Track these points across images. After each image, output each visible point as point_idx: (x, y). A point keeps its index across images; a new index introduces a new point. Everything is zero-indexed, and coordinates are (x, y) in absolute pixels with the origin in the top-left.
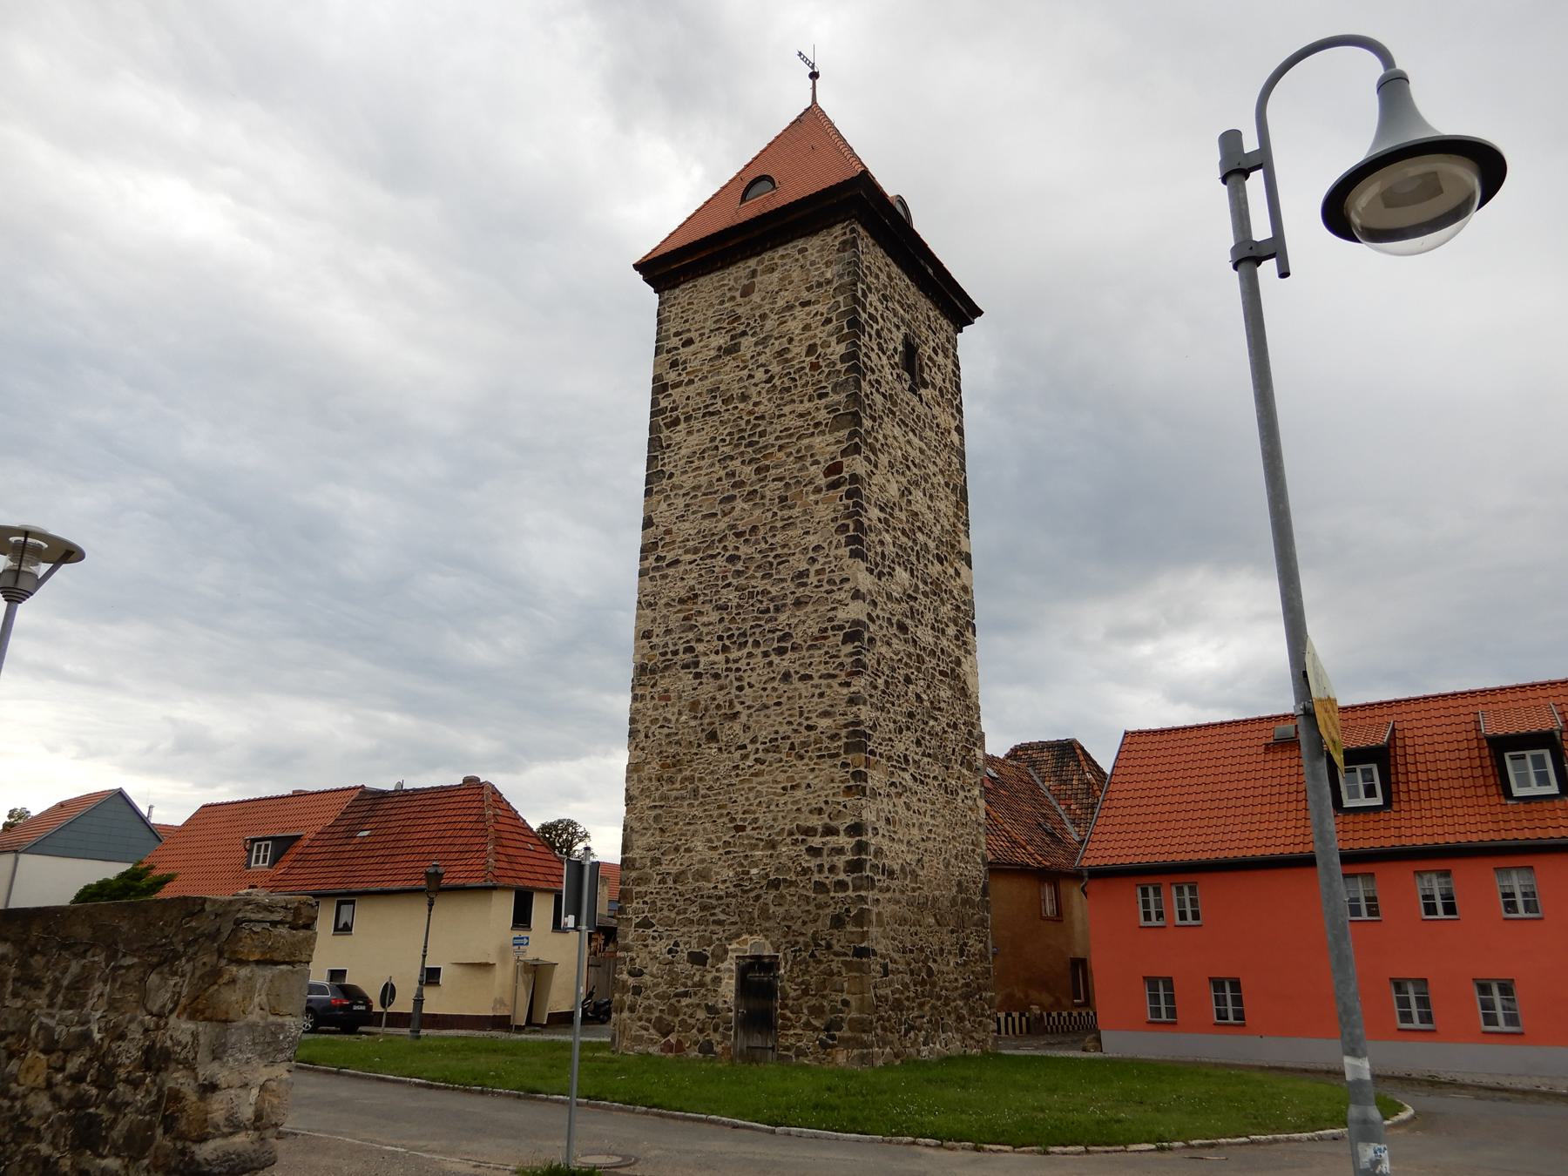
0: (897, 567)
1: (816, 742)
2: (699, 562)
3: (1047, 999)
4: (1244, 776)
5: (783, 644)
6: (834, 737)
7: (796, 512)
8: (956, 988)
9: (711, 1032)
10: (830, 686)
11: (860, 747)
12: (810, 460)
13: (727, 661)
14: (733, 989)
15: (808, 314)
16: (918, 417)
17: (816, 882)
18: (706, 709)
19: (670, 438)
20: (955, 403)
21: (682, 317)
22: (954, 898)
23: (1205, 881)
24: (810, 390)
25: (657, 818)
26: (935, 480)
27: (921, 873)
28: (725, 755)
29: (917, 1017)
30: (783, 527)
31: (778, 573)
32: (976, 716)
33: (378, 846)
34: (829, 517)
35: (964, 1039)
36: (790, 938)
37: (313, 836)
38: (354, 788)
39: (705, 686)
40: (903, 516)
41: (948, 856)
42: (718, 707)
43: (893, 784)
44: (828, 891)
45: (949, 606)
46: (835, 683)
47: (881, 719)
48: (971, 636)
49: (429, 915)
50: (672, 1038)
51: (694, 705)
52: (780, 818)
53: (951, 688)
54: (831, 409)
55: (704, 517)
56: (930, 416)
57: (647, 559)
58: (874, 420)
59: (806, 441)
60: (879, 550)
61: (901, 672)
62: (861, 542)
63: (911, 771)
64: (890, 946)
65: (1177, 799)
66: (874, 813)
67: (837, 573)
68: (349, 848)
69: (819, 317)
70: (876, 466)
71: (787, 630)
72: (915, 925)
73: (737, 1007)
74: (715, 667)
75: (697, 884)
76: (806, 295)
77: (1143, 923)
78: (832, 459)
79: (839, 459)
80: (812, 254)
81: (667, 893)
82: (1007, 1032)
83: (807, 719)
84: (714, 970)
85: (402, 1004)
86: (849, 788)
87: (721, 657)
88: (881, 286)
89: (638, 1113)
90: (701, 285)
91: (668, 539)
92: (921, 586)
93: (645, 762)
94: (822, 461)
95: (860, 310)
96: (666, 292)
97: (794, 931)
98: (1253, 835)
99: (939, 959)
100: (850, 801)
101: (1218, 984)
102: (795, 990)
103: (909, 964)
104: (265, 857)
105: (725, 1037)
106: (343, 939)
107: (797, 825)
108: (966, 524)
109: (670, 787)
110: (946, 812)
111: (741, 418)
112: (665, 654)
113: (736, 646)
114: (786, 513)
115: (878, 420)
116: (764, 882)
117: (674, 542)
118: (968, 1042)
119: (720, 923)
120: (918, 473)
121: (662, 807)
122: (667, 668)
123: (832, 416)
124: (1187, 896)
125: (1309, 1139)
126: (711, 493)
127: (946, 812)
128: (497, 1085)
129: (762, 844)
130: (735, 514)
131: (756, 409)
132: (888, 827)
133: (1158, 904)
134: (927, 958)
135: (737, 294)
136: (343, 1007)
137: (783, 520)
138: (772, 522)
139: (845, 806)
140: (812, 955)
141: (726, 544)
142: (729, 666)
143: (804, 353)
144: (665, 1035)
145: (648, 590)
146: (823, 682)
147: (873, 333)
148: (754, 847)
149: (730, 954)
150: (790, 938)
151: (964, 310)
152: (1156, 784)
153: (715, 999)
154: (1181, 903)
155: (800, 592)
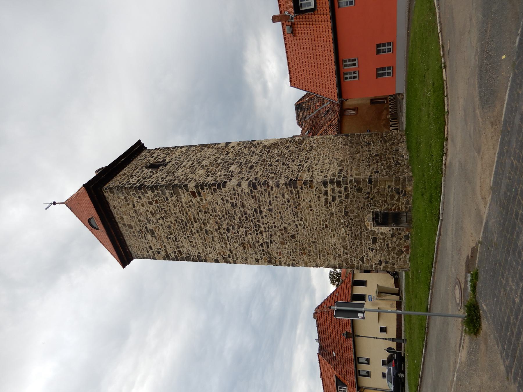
0: (230, 170)
1: (294, 199)
2: (230, 242)
3: (385, 112)
4: (304, 44)
5: (258, 211)
6: (291, 192)
7: (210, 208)
8: (382, 145)
9: (401, 236)
10: (273, 194)
11: (295, 183)
12: (191, 203)
13: (265, 231)
14: (385, 228)
15: (137, 205)
16: (176, 163)
17: (345, 198)
18: (283, 239)
19: (186, 253)
20: (172, 149)
21: (142, 250)
22: (350, 147)
23: (342, 57)
24: (165, 203)
25: (324, 256)
26: (199, 156)
27: (341, 159)
28: (300, 232)
29: (393, 160)
30: (216, 212)
31: (232, 214)
32: (284, 140)
33: (338, 349)
34: (211, 195)
35: (401, 143)
36: (366, 207)
37: (335, 372)
38: (319, 357)
39: (275, 240)
40: (211, 168)
41: (334, 149)
42: (282, 234)
43: (308, 170)
44: (348, 194)
45: (245, 150)
46: (272, 192)
47: (285, 175)
48: (256, 142)
49: (362, 336)
50: (404, 249)
51: (282, 243)
52: (322, 212)
53: (274, 149)
54: (172, 195)
55: (213, 241)
56: (175, 159)
57: (230, 261)
58: (176, 179)
59: (184, 205)
60: (223, 177)
61: (267, 168)
62: (220, 184)
63: (304, 163)
64: (368, 170)
65: (313, 67)
66: (319, 177)
67: (231, 192)
68: (339, 359)
69: (138, 201)
70: (192, 178)
71: (253, 210)
72: (360, 161)
73: (392, 226)
74: (268, 236)
75: (347, 241)
76: (131, 206)
77: (357, 79)
78: (190, 195)
79: (190, 192)
80: (116, 204)
81: (351, 252)
82: (397, 126)
83: (285, 202)
84: (378, 235)
85: (394, 345)
86: (310, 187)
87: (264, 234)
88: (127, 178)
89: (435, 270)
90: (130, 243)
91: (222, 254)
92: (237, 161)
93: (303, 260)
94: (191, 198)
95: (135, 186)
96: (133, 256)
97: (363, 206)
98: (325, 40)
99: (372, 152)
100: (315, 186)
101: (378, 52)
102: (385, 205)
103: (374, 163)
104: (343, 388)
105: (403, 230)
106: (371, 361)
107: (324, 205)
108: (215, 144)
109: (312, 251)
110: (319, 150)
111: (177, 228)
112: (264, 254)
113: (260, 228)
114: (210, 211)
115: (176, 178)
116: (346, 217)
117: (223, 251)
118: (402, 141)
119: (361, 233)
120: (196, 163)
121: (319, 254)
122: (269, 253)
123: (174, 195)
124: (348, 63)
125: (439, 10)
126: (205, 238)
127: (319, 150)
128: (425, 322)
129: (332, 218)
130: (212, 230)
131: (173, 223)
132: (324, 172)
133: (350, 74)
134: (371, 156)
135: (132, 230)
136: (395, 363)
137: (213, 212)
138: (214, 216)
139: (317, 188)
140: (372, 199)
141: (223, 233)
142: (267, 231)
143: (152, 206)
144: (402, 252)
145: (241, 261)
146: (271, 197)
147: (144, 180)
148: (333, 221)
149: (372, 229)
150: (366, 207)
151: (138, 147)
152: (308, 75)
153: (389, 234)
154: (350, 65)
155: (239, 206)
